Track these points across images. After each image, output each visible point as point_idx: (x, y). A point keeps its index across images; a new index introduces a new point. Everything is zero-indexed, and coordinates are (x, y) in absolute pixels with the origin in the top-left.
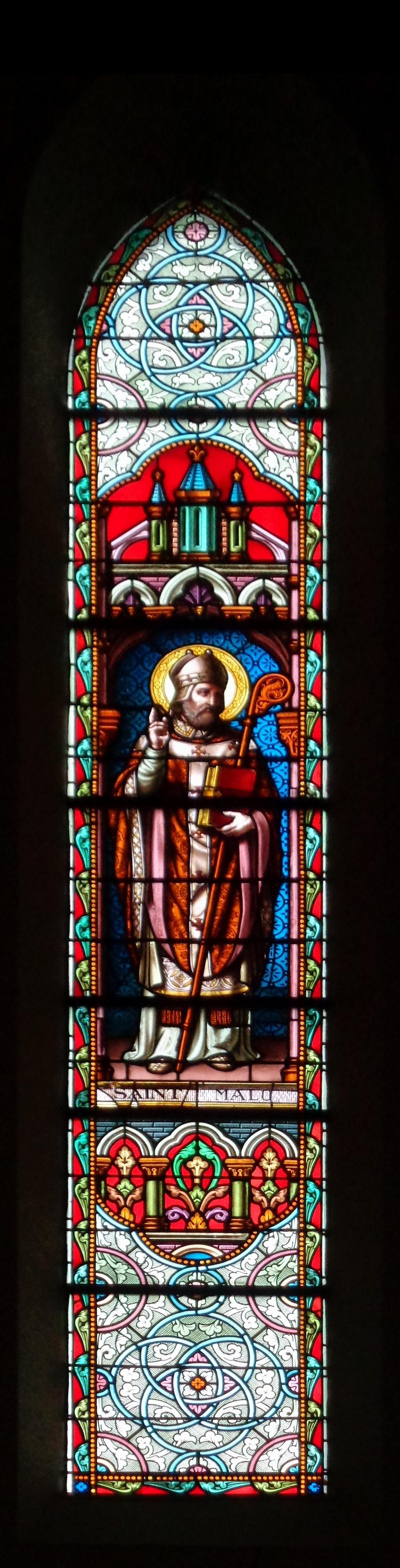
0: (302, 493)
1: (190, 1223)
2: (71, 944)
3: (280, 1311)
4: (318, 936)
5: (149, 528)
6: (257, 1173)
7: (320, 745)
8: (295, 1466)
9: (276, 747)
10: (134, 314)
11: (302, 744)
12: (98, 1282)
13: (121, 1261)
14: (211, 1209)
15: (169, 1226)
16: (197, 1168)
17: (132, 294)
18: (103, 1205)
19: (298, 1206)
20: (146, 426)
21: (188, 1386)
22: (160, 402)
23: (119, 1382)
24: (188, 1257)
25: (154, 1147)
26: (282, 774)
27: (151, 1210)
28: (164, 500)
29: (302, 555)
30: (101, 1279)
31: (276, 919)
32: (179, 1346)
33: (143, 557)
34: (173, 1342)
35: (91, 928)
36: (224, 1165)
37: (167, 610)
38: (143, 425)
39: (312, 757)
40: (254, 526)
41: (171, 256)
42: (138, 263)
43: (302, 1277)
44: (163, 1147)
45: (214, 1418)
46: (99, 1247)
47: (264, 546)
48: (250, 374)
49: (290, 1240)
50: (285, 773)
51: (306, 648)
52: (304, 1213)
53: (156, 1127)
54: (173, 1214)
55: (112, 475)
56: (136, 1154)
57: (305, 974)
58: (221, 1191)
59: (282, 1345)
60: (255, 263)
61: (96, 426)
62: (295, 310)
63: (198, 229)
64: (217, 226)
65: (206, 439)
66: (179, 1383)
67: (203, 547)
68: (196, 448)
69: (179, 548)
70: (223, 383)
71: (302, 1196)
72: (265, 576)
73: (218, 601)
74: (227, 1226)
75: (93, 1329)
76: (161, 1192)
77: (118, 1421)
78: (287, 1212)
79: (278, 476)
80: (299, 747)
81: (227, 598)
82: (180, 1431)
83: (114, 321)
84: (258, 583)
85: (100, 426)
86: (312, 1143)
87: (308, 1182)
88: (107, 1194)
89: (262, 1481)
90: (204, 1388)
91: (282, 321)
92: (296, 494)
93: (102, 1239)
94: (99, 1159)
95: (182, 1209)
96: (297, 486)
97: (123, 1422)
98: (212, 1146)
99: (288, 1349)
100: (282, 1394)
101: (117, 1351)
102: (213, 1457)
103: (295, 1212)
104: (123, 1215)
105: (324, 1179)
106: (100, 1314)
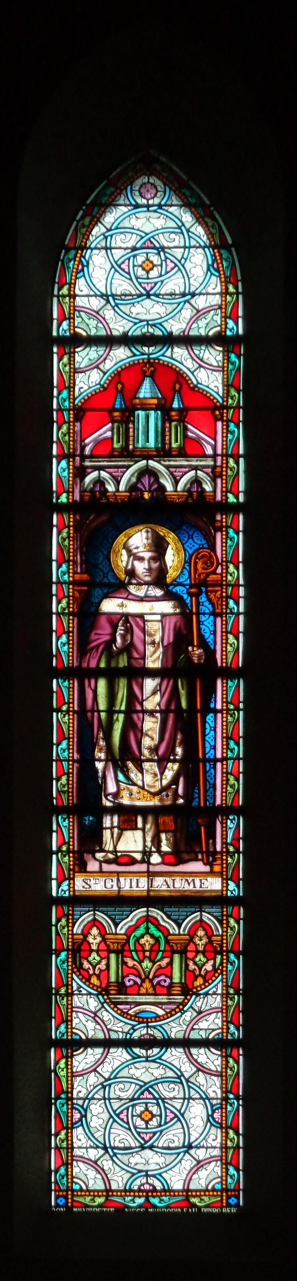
0: (225, 399)
1: (142, 988)
2: (55, 413)
3: (208, 1058)
4: (235, 582)
5: (112, 429)
6: (191, 947)
7: (237, 603)
8: (218, 1183)
9: (205, 604)
10: (100, 1106)
11: (224, 603)
12: (75, 1037)
13: (92, 1168)
14: (158, 976)
15: (126, 990)
16: (147, 944)
17: (100, 241)
18: (78, 973)
19: (222, 973)
20: (110, 350)
21: (139, 1118)
22: (121, 330)
23: (89, 1115)
24: (139, 1015)
25: (116, 928)
26: (209, 626)
27: (113, 978)
28: (123, 406)
29: (224, 451)
30: (76, 1034)
31: (206, 742)
32: (134, 236)
33: (107, 452)
34: (129, 1082)
35: (69, 644)
36: (167, 942)
37: (124, 496)
38: (108, 349)
39: (232, 613)
40: (189, 426)
41: (128, 358)
42: (105, 216)
43: (225, 1031)
44: (122, 929)
45: (160, 295)
46: (75, 1007)
47: (197, 442)
48: (187, 305)
49: (216, 1002)
50: (212, 740)
51: (227, 527)
52: (227, 979)
53: (115, 911)
54: (129, 981)
55: (86, 387)
56: (103, 933)
57: (227, 751)
58: (166, 961)
59: (209, 1085)
60: (191, 216)
61: (74, 350)
62: (221, 255)
63: (149, 189)
64: (163, 186)
65: (154, 359)
66: (134, 266)
67: (152, 444)
68: (148, 366)
69: (134, 445)
70: (168, 313)
71: (225, 965)
72: (196, 468)
73: (162, 488)
74: (169, 991)
75: (72, 370)
76: (120, 962)
77: (90, 298)
78: (214, 978)
79: (208, 387)
80: (222, 605)
81: (169, 487)
82: (134, 1154)
83: (88, 263)
84: (192, 473)
85: (77, 350)
86: (232, 922)
87: (228, 1130)
88: (82, 964)
89: (194, 1197)
90: (152, 269)
91: (210, 262)
92: (221, 401)
93: (77, 1001)
94: (76, 937)
95: (136, 976)
96: (221, 394)
97: (94, 298)
98: (158, 926)
99: (214, 1088)
100: (209, 273)
101: (87, 1090)
102: (158, 1028)
103: (220, 977)
104: (92, 981)
105: (241, 456)
106: (78, 358)
